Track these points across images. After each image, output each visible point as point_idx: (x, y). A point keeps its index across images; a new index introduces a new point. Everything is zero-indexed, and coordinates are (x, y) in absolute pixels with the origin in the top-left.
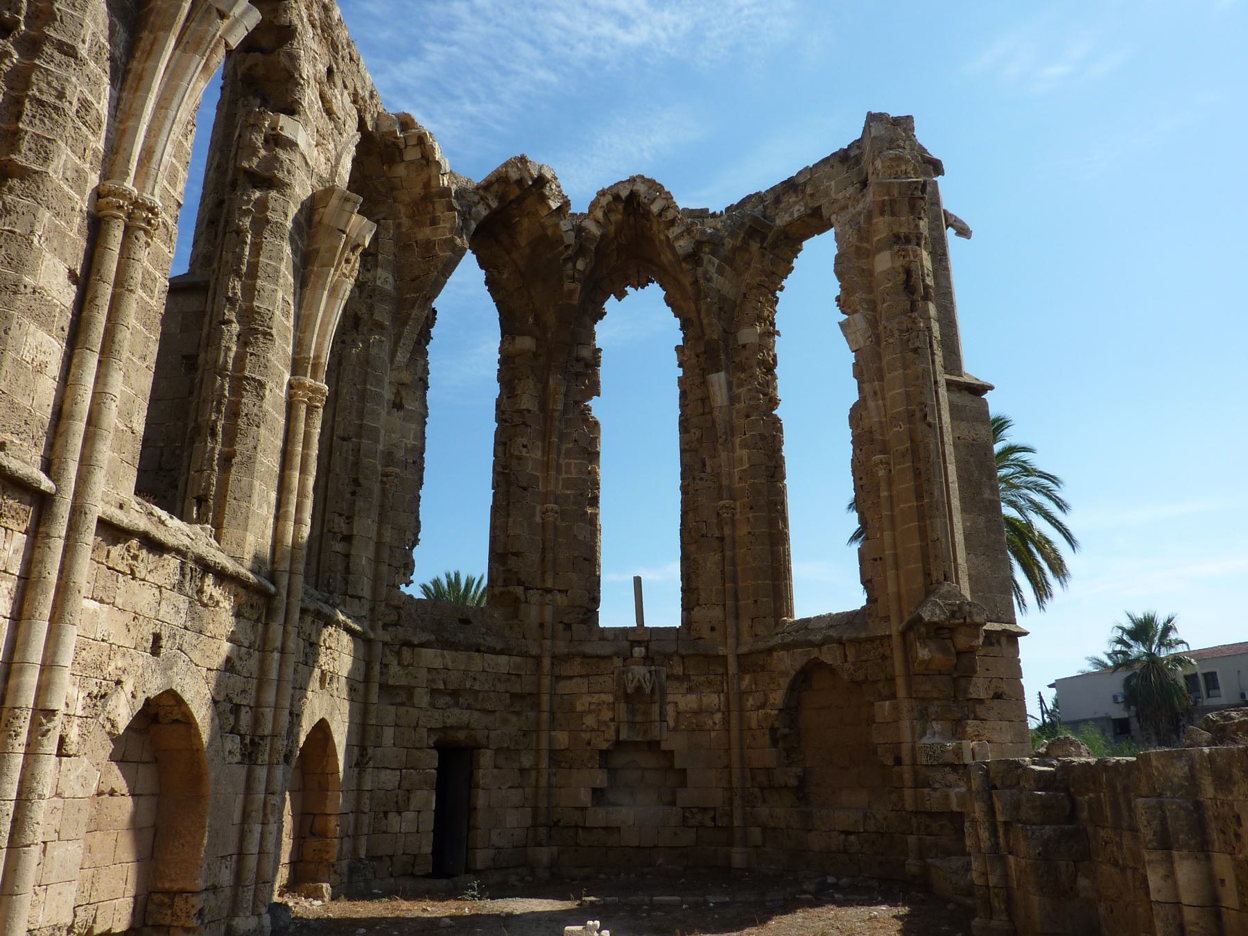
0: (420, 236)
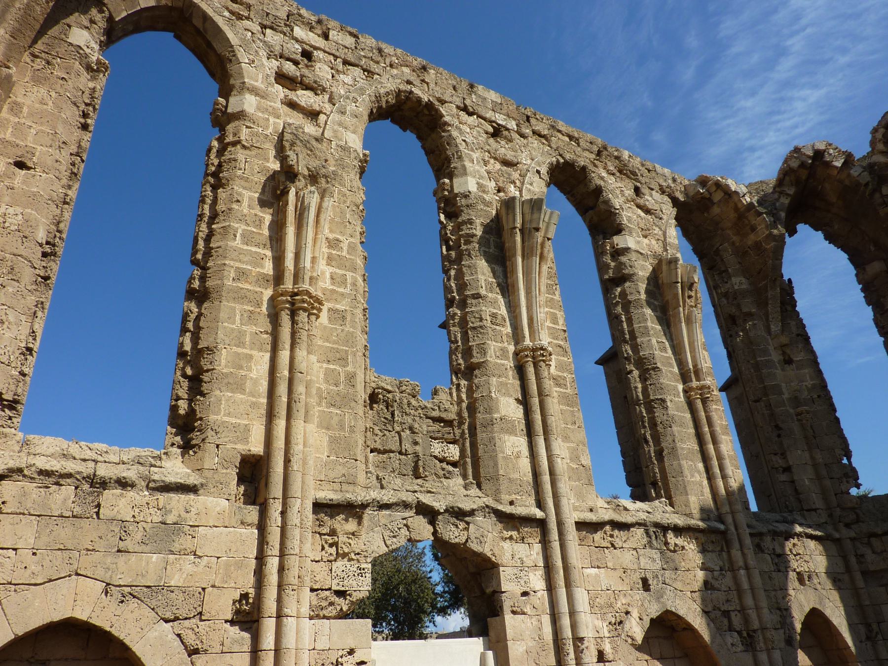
0: (750, 243)
